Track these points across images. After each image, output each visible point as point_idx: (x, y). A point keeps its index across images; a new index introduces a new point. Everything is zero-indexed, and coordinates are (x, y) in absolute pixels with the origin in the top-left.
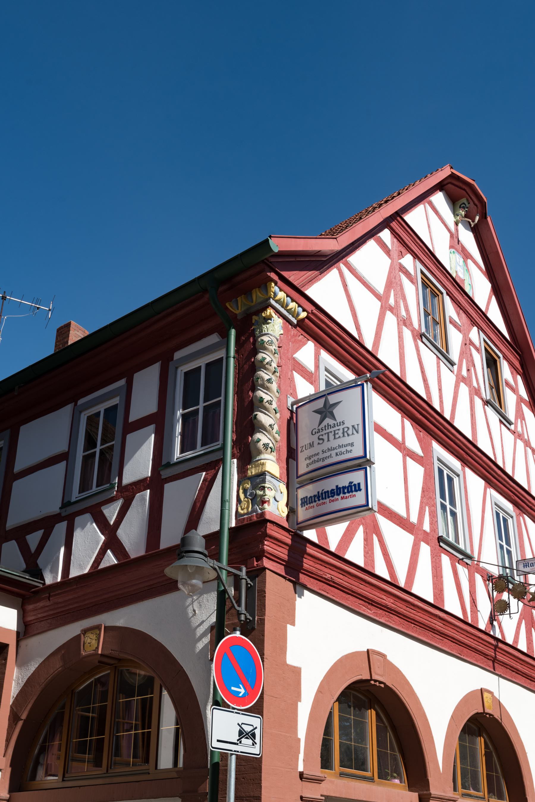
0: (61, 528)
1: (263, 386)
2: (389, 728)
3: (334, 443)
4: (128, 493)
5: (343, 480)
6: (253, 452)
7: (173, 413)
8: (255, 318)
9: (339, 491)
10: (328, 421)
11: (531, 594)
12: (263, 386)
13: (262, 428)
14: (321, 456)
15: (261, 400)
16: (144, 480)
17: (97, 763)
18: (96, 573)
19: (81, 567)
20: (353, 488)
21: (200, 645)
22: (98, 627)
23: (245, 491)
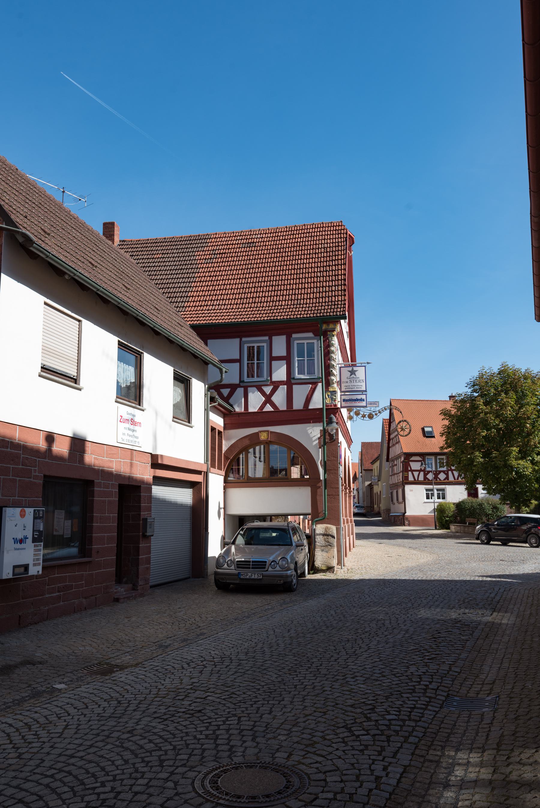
0: (240, 391)
1: (333, 360)
2: (209, 354)
3: (356, 384)
4: (276, 385)
5: (359, 397)
6: (331, 382)
7: (294, 359)
8: (329, 333)
9: (357, 400)
10: (353, 376)
11: (473, 493)
12: (333, 360)
13: (334, 375)
14: (351, 387)
15: (334, 365)
16: (283, 381)
17: (355, 515)
18: (261, 412)
19: (254, 408)
20: (362, 400)
21: (315, 443)
22: (268, 431)
23: (328, 395)
